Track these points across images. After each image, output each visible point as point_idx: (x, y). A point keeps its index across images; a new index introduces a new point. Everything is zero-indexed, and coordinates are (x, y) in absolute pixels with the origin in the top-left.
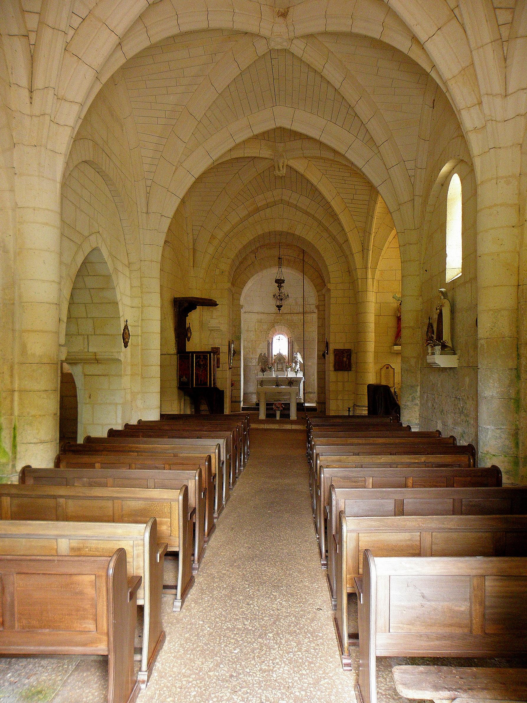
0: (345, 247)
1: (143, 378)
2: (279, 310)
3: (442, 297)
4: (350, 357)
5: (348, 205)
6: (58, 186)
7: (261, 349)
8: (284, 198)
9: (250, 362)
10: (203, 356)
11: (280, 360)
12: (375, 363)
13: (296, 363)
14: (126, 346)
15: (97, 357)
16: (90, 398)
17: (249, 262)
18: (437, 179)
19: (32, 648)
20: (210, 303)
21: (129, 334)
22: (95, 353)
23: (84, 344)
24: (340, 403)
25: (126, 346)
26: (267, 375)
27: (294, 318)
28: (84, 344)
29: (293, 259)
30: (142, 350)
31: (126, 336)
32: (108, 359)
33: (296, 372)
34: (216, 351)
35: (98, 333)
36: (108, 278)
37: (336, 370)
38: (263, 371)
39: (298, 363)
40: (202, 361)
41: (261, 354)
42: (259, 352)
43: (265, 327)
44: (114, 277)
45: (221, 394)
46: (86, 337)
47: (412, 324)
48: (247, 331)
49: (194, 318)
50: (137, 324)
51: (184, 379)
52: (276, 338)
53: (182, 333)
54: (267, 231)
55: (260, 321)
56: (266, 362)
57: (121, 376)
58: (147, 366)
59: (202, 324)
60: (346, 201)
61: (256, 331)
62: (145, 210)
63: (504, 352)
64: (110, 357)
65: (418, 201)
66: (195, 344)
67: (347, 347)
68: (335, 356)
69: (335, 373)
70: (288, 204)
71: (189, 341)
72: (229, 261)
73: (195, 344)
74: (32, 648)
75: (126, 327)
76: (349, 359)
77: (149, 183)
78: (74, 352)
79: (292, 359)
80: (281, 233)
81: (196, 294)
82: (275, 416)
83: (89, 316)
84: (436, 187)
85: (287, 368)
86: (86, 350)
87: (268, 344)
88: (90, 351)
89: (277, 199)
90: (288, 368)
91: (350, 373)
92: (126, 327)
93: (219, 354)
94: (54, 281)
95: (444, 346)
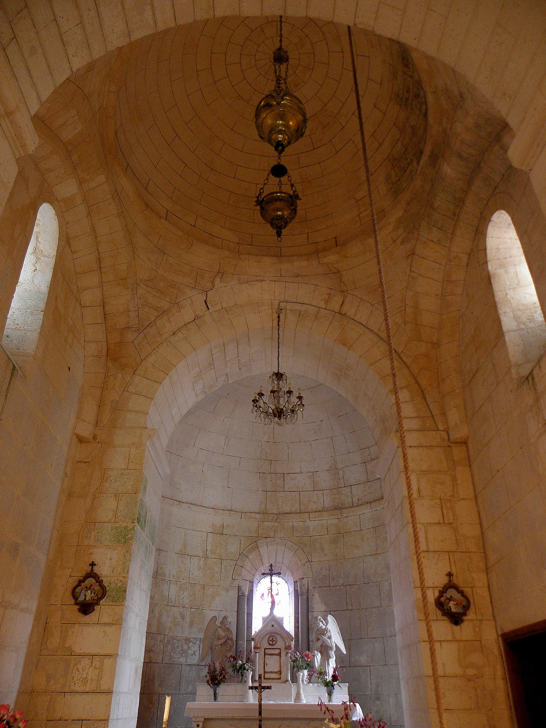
7: (221, 606)
9: (184, 652)
11: (272, 641)
13: (325, 650)
17: (187, 315)
19: (404, 697)
27: (308, 523)
33: (329, 686)
38: (215, 680)
39: (332, 653)
43: (233, 548)
48: (182, 554)
52: (262, 586)
55: (219, 532)
61: (206, 557)
74: (404, 697)
79: (308, 635)
85: (296, 668)
87: (240, 597)
90: (300, 668)
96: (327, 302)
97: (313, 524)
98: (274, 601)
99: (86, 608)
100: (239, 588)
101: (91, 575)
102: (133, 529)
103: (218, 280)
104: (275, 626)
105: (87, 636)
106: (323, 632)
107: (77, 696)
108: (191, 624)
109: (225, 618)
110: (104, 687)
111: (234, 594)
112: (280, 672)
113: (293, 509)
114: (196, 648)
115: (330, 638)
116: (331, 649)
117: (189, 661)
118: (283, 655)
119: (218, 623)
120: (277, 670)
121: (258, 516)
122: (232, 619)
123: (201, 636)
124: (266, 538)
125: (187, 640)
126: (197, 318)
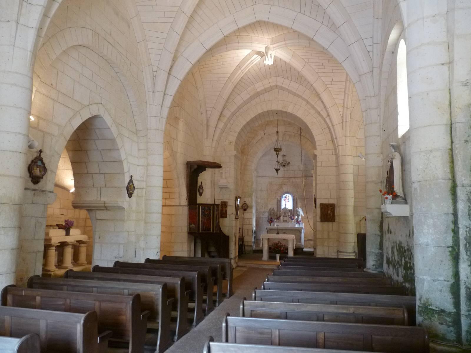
0: (327, 120)
1: (146, 223)
2: (277, 172)
3: (393, 150)
4: (334, 210)
5: (328, 86)
6: (29, 54)
7: (272, 205)
8: (278, 84)
9: (263, 215)
10: (208, 207)
12: (355, 216)
14: (130, 195)
15: (106, 205)
16: (100, 238)
17: (259, 137)
18: (388, 47)
20: (218, 166)
21: (134, 187)
22: (105, 202)
23: (97, 195)
24: (326, 249)
25: (130, 195)
26: (272, 227)
28: (97, 195)
29: (293, 134)
30: (146, 200)
31: (130, 190)
32: (114, 207)
34: (224, 204)
35: (108, 186)
36: (113, 140)
37: (322, 221)
40: (207, 211)
41: (271, 208)
42: (270, 206)
44: (118, 141)
45: (226, 239)
46: (99, 189)
47: (374, 179)
49: (205, 178)
50: (142, 179)
51: (193, 226)
53: (193, 189)
54: (265, 110)
55: (271, 184)
56: (276, 215)
57: (123, 220)
58: (151, 213)
59: (213, 183)
60: (326, 83)
62: (151, 90)
63: (438, 196)
64: (115, 205)
65: (376, 71)
66: (206, 198)
67: (331, 202)
68: (321, 209)
69: (321, 223)
70: (282, 88)
71: (201, 195)
72: (236, 134)
73: (206, 198)
75: (131, 181)
76: (333, 212)
77: (155, 69)
78: (90, 201)
80: (277, 112)
81: (209, 159)
82: (275, 258)
83: (101, 172)
84: (387, 55)
86: (99, 199)
88: (101, 200)
89: (272, 84)
91: (335, 224)
92: (131, 181)
93: (227, 207)
94: (19, 133)
95: (395, 197)
96: (297, 132)
97: (299, 180)
98: (288, 203)
99: (245, 210)
100: (277, 198)
101: (245, 204)
102: (252, 194)
103: (267, 127)
104: (286, 210)
105: (246, 215)
106: (298, 212)
107: (8, 203)
108: (265, 208)
109: (273, 208)
110: (250, 224)
111: (276, 200)
112: (287, 220)
113: (293, 176)
114: (266, 213)
115: (299, 213)
116: (300, 215)
117: (265, 217)
118: (288, 217)
119: (272, 209)
120: (286, 220)
121: (282, 178)
122: (276, 210)
123: (268, 211)
124: (284, 185)
125: (264, 212)
126: (262, 138)
